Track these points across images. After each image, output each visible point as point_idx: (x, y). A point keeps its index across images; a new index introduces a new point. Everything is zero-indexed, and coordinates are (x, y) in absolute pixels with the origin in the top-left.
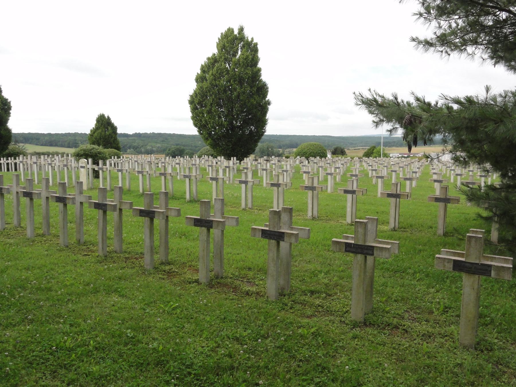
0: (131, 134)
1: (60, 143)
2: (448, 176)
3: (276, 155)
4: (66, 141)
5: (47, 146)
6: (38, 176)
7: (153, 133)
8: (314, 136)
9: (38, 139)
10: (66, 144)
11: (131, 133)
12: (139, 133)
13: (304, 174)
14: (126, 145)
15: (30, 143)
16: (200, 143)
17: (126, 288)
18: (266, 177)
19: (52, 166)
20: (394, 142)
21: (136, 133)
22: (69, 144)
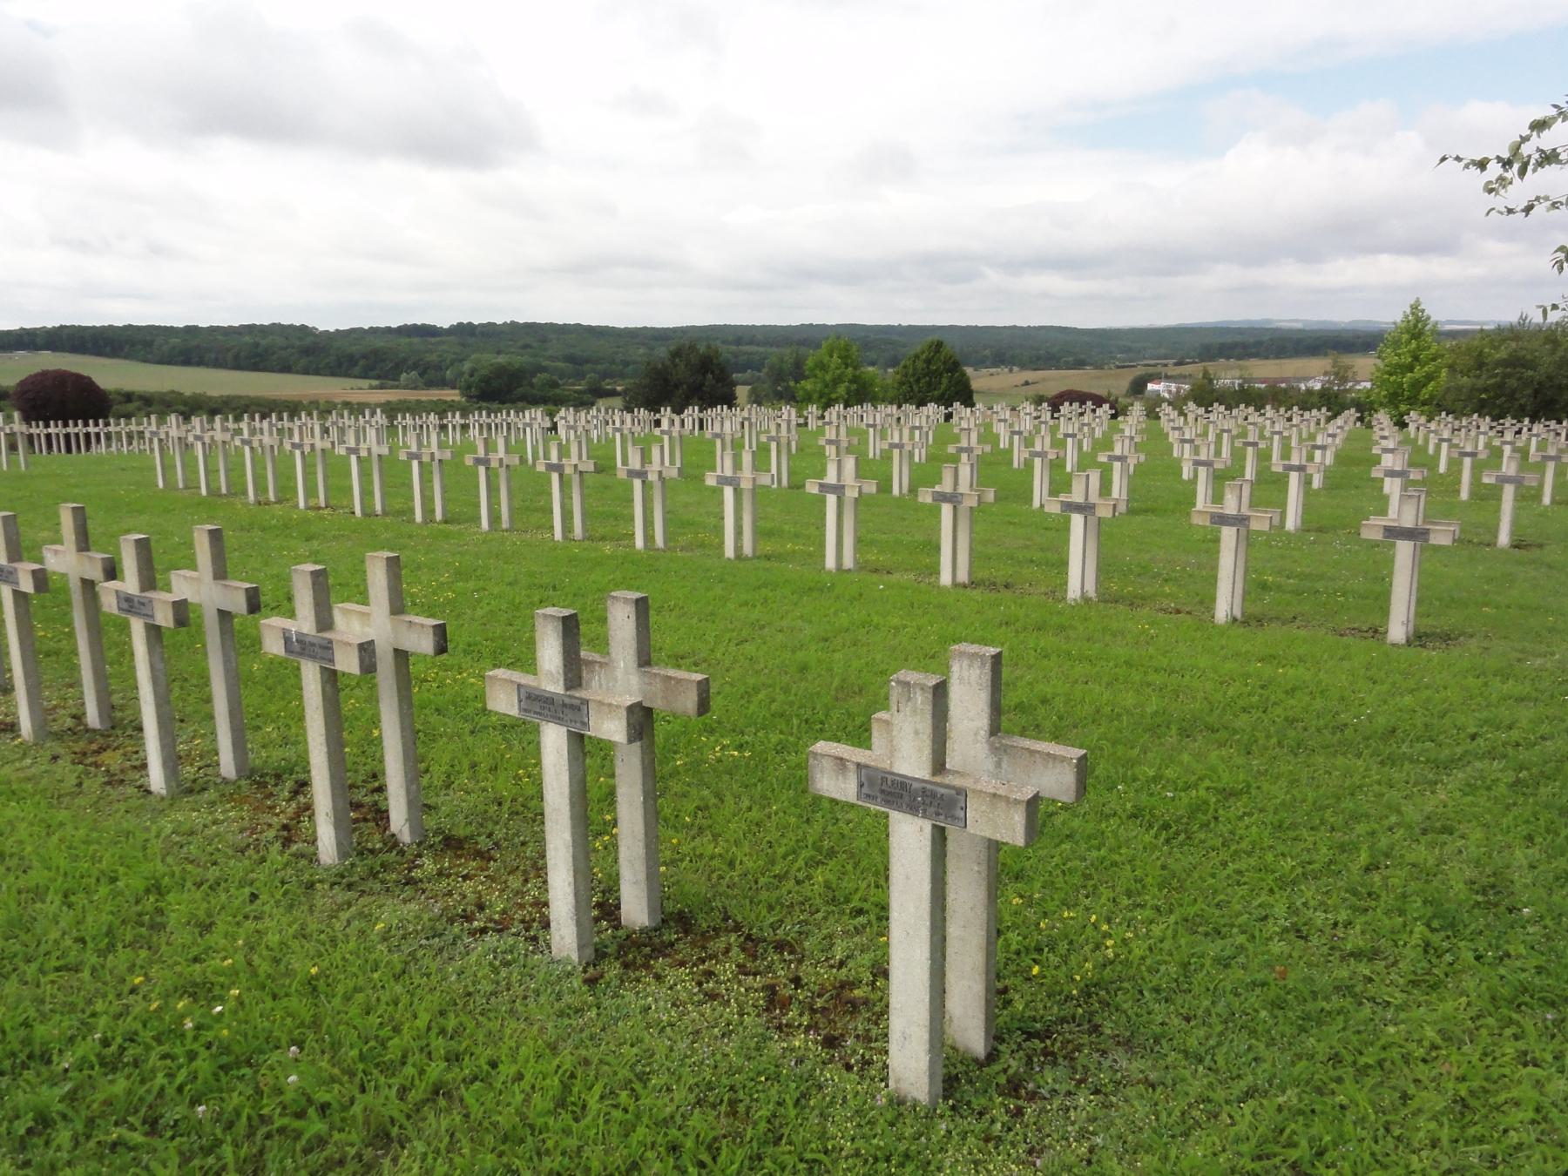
0: (446, 326)
1: (213, 356)
2: (1431, 450)
3: (1525, 398)
4: (228, 350)
5: (176, 364)
6: (227, 477)
7: (513, 323)
8: (1014, 327)
9: (148, 344)
10: (230, 356)
11: (445, 322)
12: (470, 324)
13: (1387, 480)
14: (405, 360)
15: (126, 357)
16: (641, 351)
17: (483, 931)
18: (779, 452)
19: (420, 463)
20: (1259, 343)
21: (460, 324)
22: (236, 357)
